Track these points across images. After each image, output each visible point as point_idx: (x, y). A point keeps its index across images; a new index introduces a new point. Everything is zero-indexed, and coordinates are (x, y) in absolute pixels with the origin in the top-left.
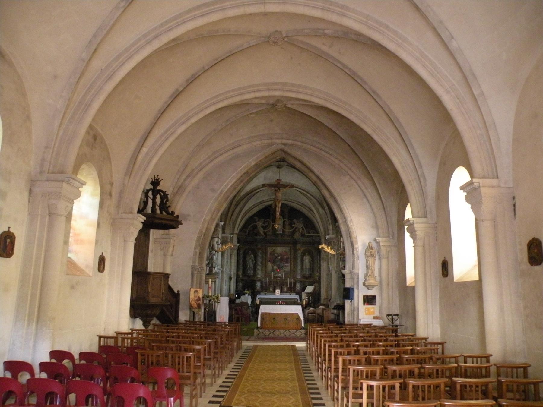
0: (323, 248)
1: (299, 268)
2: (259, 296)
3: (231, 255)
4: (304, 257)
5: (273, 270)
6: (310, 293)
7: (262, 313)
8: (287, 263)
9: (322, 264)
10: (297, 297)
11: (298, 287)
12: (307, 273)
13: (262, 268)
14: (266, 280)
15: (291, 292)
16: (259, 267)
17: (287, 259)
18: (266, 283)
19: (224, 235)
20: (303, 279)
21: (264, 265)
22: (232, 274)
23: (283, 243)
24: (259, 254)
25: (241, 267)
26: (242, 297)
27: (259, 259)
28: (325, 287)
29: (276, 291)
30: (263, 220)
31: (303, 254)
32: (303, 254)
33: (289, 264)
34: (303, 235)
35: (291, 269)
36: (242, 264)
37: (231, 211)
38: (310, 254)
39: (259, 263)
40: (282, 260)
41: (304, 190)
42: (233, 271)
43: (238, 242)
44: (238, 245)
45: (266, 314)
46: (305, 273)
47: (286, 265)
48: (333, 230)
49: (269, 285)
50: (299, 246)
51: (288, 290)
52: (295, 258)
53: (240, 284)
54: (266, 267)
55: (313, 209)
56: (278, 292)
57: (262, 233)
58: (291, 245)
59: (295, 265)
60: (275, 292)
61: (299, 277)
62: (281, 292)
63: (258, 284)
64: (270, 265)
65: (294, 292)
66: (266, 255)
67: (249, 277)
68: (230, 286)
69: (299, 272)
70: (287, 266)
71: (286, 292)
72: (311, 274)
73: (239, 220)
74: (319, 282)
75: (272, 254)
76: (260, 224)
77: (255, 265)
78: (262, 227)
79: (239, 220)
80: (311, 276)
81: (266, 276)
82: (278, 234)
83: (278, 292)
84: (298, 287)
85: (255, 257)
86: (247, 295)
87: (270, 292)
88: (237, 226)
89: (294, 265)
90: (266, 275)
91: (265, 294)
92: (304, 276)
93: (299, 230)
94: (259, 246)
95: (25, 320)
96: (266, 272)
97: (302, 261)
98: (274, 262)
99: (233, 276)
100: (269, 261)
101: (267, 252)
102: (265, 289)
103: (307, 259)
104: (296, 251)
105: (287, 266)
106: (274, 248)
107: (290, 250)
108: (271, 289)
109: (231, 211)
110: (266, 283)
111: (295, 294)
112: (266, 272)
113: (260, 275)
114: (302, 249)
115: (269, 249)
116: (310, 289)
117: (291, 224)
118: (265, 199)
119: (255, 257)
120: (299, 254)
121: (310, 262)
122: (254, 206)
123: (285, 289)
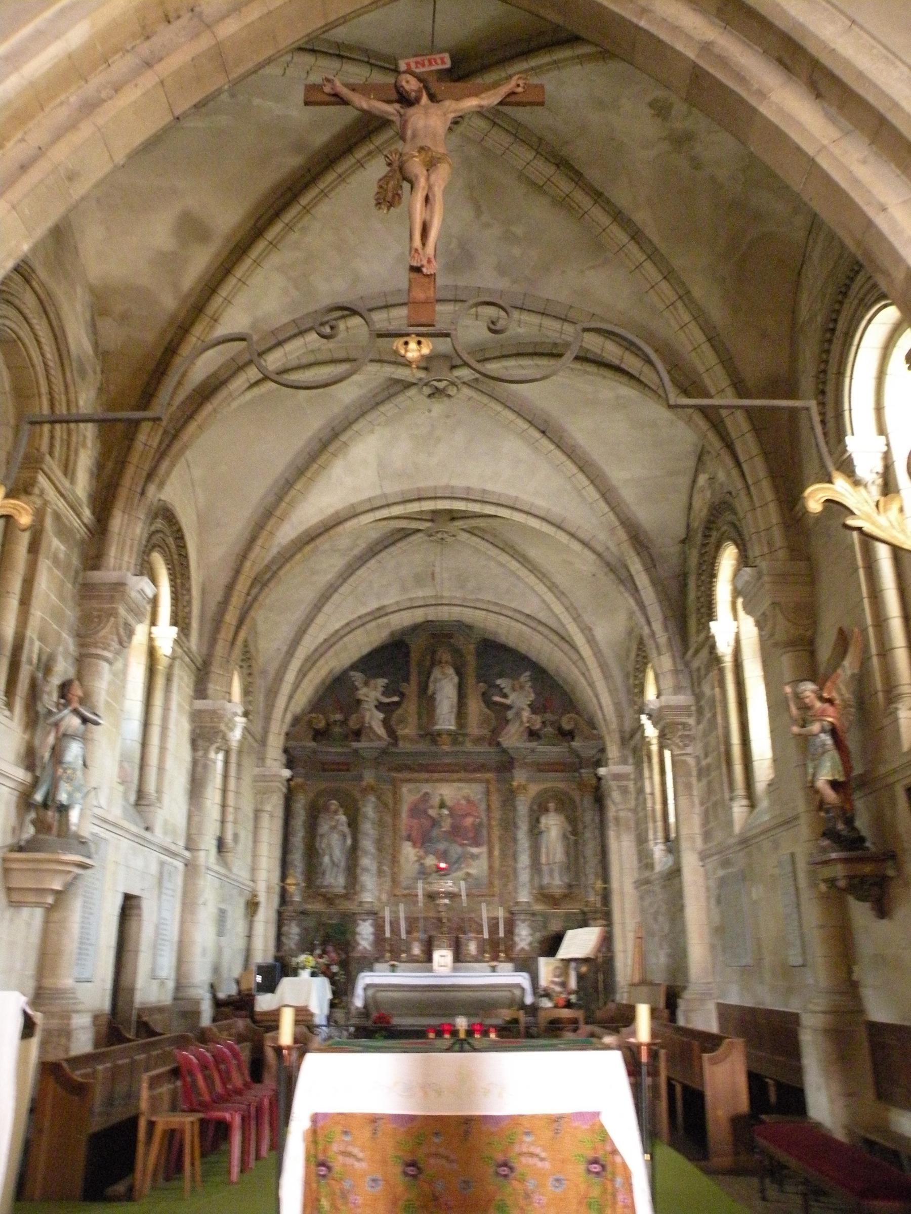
0: (834, 507)
1: (524, 860)
2: (365, 979)
3: (257, 813)
4: (543, 820)
5: (424, 873)
6: (586, 960)
7: (316, 1118)
8: (477, 844)
9: (613, 844)
10: (523, 979)
11: (524, 937)
12: (556, 882)
13: (380, 864)
14: (395, 913)
15: (495, 958)
16: (367, 861)
17: (477, 828)
18: (395, 930)
19: (200, 704)
20: (538, 907)
21: (389, 856)
22: (261, 888)
23: (464, 769)
24: (369, 809)
25: (297, 857)
26: (286, 984)
27: (368, 828)
28: (631, 936)
29: (437, 955)
30: (382, 682)
31: (539, 809)
32: (539, 809)
33: (482, 850)
34: (533, 734)
35: (491, 867)
36: (301, 849)
37: (236, 600)
38: (565, 805)
39: (368, 844)
40: (456, 832)
41: (543, 519)
42: (262, 875)
43: (289, 765)
44: (287, 773)
45: (346, 1122)
46: (546, 880)
47: (475, 850)
48: (676, 672)
49: (409, 932)
50: (520, 777)
51: (481, 950)
52: (509, 826)
53: (294, 930)
54: (394, 860)
55: (573, 630)
56: (443, 957)
57: (381, 731)
58: (489, 775)
59: (509, 854)
60: (429, 959)
61: (524, 896)
62: (458, 958)
63: (365, 932)
64: (409, 852)
65: (509, 959)
66: (396, 814)
67: (329, 900)
68: (249, 937)
69: (524, 876)
70: (474, 857)
71: (477, 960)
72: (570, 886)
73: (290, 676)
74: (605, 916)
75: (418, 811)
76: (371, 693)
77: (353, 852)
78: (380, 706)
79: (290, 676)
80: (570, 893)
81: (394, 898)
82: (439, 734)
83: (443, 957)
84: (524, 937)
85: (353, 824)
86: (305, 974)
87: (413, 960)
88: (281, 701)
89: (502, 851)
90: (399, 894)
91: (393, 968)
92: (545, 896)
93: (518, 715)
94: (369, 777)
95: (407, 919)
96: (395, 881)
97: (535, 832)
98: (423, 840)
99: (262, 898)
100: (409, 838)
101: (397, 800)
102: (389, 950)
103: (553, 826)
104: (509, 799)
105: (474, 857)
106: (426, 788)
107: (488, 793)
108: (416, 950)
109: (236, 600)
110: (395, 924)
111: (510, 966)
112: (395, 881)
113: (371, 890)
114: (534, 789)
115: (405, 789)
116: (580, 943)
117: (486, 698)
118: (386, 602)
119: (353, 824)
120: (523, 807)
121: (565, 837)
122: (349, 628)
123: (472, 948)
